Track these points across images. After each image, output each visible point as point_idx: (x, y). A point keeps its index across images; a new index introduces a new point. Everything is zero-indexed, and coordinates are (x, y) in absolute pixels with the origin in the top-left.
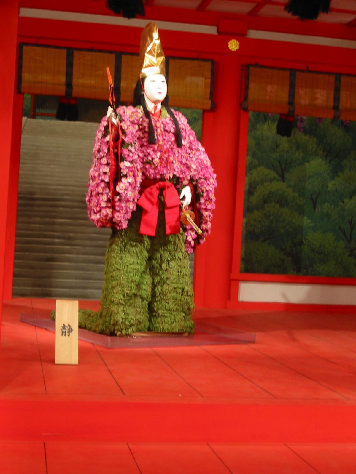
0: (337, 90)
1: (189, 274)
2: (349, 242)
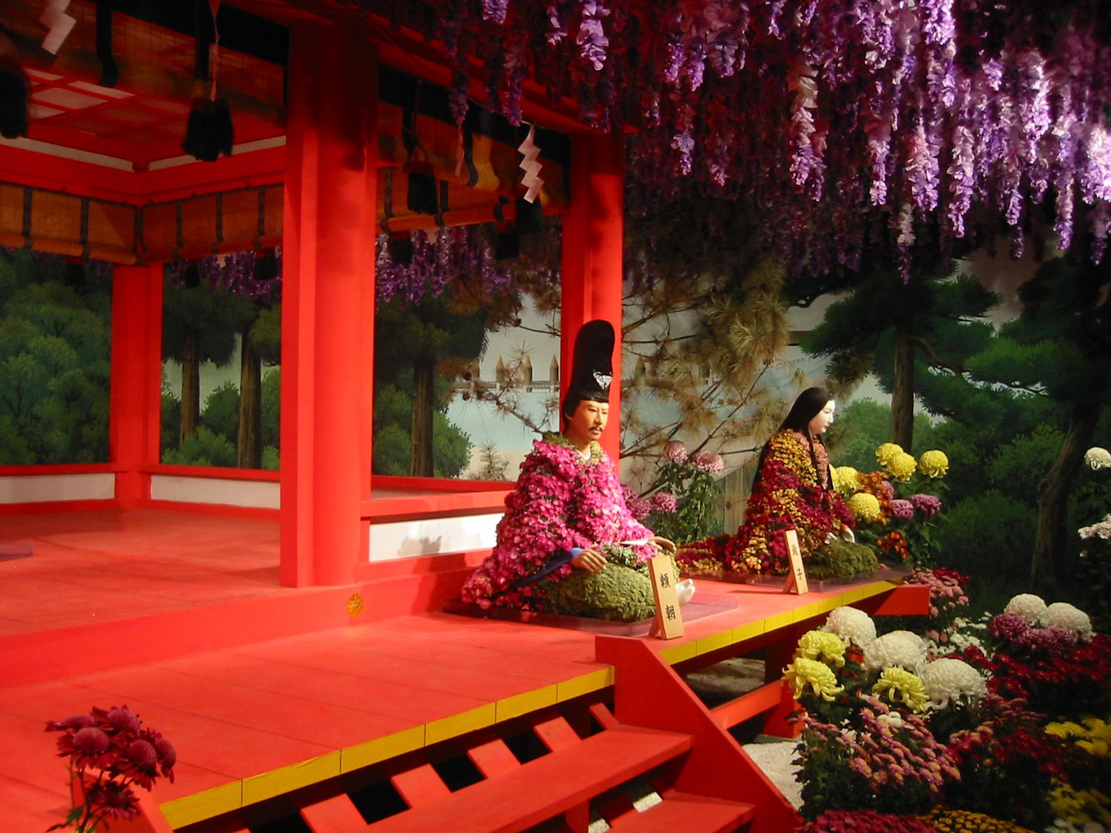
0: (28, 209)
1: (543, 372)
2: (17, 416)
